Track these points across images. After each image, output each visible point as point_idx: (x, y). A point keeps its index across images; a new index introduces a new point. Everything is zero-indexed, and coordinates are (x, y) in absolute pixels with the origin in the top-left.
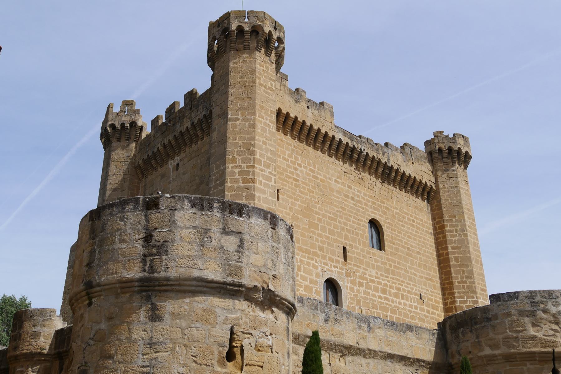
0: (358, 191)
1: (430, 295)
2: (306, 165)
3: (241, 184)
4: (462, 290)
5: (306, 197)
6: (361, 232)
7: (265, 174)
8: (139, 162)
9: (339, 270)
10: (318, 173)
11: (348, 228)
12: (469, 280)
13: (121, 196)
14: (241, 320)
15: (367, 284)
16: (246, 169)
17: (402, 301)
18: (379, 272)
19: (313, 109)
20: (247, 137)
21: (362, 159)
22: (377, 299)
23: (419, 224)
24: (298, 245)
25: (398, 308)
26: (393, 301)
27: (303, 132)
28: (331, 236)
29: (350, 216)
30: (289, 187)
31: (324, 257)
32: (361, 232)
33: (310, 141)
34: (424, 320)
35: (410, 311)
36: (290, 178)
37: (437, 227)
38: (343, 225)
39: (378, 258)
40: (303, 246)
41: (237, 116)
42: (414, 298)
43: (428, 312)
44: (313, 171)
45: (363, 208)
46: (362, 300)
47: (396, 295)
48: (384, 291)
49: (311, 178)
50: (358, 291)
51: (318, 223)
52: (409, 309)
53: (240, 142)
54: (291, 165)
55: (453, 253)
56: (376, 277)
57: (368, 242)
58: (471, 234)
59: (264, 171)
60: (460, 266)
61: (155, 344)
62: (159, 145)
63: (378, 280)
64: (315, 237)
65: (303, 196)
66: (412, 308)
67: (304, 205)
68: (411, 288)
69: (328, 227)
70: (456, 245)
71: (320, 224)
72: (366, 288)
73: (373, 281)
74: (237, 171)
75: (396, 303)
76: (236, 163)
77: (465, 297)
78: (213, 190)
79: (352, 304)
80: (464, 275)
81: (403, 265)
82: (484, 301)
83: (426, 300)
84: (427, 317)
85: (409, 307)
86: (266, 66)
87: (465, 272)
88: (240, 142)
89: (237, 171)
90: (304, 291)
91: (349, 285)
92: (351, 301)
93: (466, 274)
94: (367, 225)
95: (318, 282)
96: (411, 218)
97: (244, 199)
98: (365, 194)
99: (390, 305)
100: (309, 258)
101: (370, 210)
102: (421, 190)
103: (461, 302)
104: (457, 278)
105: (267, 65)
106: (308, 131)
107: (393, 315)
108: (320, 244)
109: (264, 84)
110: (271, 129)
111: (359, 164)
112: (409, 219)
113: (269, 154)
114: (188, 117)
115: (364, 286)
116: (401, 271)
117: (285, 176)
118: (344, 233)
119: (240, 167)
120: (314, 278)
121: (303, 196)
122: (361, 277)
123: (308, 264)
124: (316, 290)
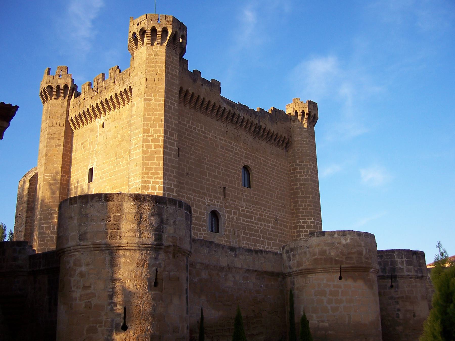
0: (236, 145)
1: (283, 218)
2: (200, 129)
3: (153, 149)
4: (305, 214)
5: (199, 152)
6: (237, 176)
7: (171, 141)
8: (72, 117)
9: (220, 204)
10: (208, 134)
11: (228, 173)
12: (309, 207)
13: (58, 144)
14: (161, 264)
15: (239, 213)
16: (157, 138)
17: (263, 223)
18: (248, 204)
19: (206, 86)
20: (158, 113)
21: (240, 121)
22: (269, 158)
23: (278, 167)
24: (192, 188)
25: (260, 228)
26: (256, 224)
27: (198, 104)
28: (215, 180)
29: (229, 164)
30: (187, 146)
31: (210, 196)
32: (237, 176)
33: (203, 110)
34: (277, 235)
35: (268, 230)
36: (187, 139)
37: (291, 169)
38: (224, 172)
39: (248, 194)
40: (195, 189)
41: (150, 97)
42: (271, 221)
43: (281, 230)
44: (204, 133)
45: (239, 158)
46: (235, 224)
47: (259, 220)
48: (251, 217)
49: (203, 138)
50: (233, 218)
51: (206, 171)
52: (268, 228)
53: (153, 117)
54: (189, 129)
55: (301, 188)
56: (246, 208)
57: (241, 183)
58: (313, 175)
59: (170, 139)
60: (304, 197)
61: (115, 280)
62: (89, 107)
63: (247, 209)
64: (204, 181)
65: (196, 152)
66: (270, 228)
67: (197, 159)
68: (269, 214)
69: (213, 174)
70: (303, 183)
71: (208, 172)
72: (239, 216)
73: (243, 211)
74: (150, 139)
75: (259, 225)
76: (150, 133)
77: (306, 219)
78: (133, 152)
79: (228, 227)
80: (307, 204)
81: (265, 198)
82: (318, 222)
83: (280, 222)
84: (279, 233)
85: (268, 227)
86: (172, 58)
87: (307, 201)
88: (153, 117)
89: (150, 139)
90: (196, 220)
91: (227, 214)
92: (228, 226)
93: (308, 203)
94: (241, 170)
95: (206, 213)
96: (273, 163)
97: (155, 160)
98: (241, 148)
99: (255, 227)
100: (200, 197)
101: (244, 159)
102: (281, 142)
103: (303, 222)
104: (302, 206)
105: (173, 57)
106: (202, 103)
107: (256, 233)
108: (208, 186)
109: (171, 72)
110: (175, 107)
111: (238, 125)
112: (271, 164)
113: (173, 125)
114: (112, 88)
115: (237, 214)
116: (263, 202)
117: (184, 138)
118: (224, 177)
119: (152, 136)
120: (203, 211)
121: (196, 152)
122: (235, 208)
123: (199, 201)
124: (203, 219)
